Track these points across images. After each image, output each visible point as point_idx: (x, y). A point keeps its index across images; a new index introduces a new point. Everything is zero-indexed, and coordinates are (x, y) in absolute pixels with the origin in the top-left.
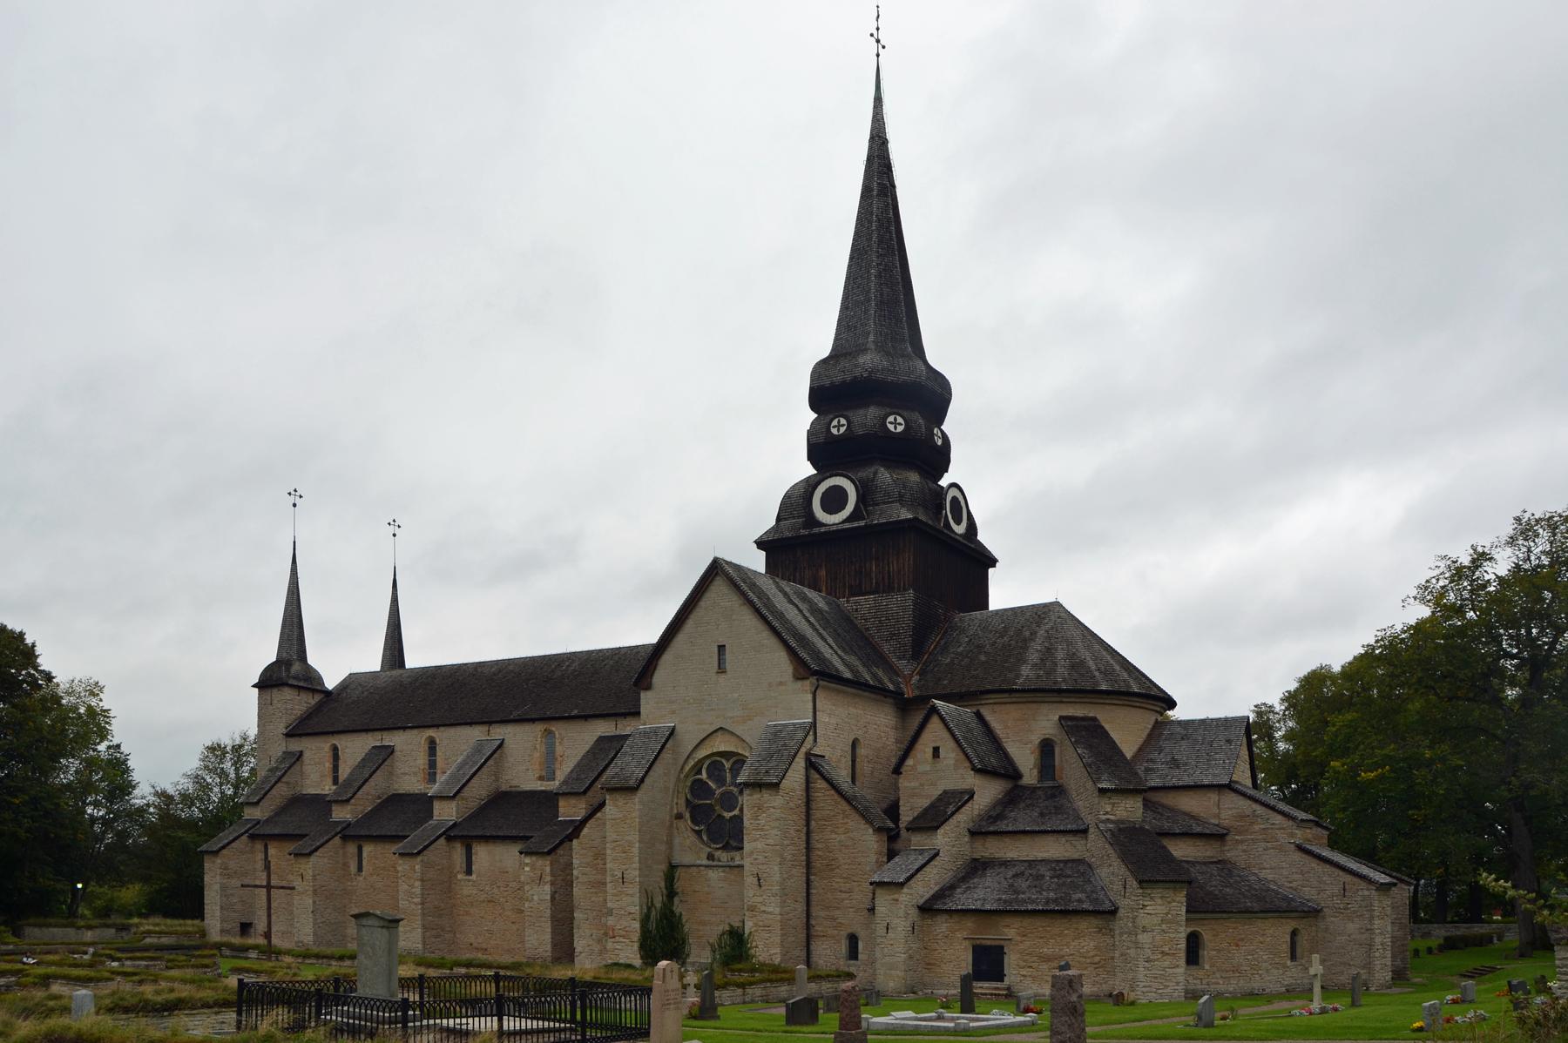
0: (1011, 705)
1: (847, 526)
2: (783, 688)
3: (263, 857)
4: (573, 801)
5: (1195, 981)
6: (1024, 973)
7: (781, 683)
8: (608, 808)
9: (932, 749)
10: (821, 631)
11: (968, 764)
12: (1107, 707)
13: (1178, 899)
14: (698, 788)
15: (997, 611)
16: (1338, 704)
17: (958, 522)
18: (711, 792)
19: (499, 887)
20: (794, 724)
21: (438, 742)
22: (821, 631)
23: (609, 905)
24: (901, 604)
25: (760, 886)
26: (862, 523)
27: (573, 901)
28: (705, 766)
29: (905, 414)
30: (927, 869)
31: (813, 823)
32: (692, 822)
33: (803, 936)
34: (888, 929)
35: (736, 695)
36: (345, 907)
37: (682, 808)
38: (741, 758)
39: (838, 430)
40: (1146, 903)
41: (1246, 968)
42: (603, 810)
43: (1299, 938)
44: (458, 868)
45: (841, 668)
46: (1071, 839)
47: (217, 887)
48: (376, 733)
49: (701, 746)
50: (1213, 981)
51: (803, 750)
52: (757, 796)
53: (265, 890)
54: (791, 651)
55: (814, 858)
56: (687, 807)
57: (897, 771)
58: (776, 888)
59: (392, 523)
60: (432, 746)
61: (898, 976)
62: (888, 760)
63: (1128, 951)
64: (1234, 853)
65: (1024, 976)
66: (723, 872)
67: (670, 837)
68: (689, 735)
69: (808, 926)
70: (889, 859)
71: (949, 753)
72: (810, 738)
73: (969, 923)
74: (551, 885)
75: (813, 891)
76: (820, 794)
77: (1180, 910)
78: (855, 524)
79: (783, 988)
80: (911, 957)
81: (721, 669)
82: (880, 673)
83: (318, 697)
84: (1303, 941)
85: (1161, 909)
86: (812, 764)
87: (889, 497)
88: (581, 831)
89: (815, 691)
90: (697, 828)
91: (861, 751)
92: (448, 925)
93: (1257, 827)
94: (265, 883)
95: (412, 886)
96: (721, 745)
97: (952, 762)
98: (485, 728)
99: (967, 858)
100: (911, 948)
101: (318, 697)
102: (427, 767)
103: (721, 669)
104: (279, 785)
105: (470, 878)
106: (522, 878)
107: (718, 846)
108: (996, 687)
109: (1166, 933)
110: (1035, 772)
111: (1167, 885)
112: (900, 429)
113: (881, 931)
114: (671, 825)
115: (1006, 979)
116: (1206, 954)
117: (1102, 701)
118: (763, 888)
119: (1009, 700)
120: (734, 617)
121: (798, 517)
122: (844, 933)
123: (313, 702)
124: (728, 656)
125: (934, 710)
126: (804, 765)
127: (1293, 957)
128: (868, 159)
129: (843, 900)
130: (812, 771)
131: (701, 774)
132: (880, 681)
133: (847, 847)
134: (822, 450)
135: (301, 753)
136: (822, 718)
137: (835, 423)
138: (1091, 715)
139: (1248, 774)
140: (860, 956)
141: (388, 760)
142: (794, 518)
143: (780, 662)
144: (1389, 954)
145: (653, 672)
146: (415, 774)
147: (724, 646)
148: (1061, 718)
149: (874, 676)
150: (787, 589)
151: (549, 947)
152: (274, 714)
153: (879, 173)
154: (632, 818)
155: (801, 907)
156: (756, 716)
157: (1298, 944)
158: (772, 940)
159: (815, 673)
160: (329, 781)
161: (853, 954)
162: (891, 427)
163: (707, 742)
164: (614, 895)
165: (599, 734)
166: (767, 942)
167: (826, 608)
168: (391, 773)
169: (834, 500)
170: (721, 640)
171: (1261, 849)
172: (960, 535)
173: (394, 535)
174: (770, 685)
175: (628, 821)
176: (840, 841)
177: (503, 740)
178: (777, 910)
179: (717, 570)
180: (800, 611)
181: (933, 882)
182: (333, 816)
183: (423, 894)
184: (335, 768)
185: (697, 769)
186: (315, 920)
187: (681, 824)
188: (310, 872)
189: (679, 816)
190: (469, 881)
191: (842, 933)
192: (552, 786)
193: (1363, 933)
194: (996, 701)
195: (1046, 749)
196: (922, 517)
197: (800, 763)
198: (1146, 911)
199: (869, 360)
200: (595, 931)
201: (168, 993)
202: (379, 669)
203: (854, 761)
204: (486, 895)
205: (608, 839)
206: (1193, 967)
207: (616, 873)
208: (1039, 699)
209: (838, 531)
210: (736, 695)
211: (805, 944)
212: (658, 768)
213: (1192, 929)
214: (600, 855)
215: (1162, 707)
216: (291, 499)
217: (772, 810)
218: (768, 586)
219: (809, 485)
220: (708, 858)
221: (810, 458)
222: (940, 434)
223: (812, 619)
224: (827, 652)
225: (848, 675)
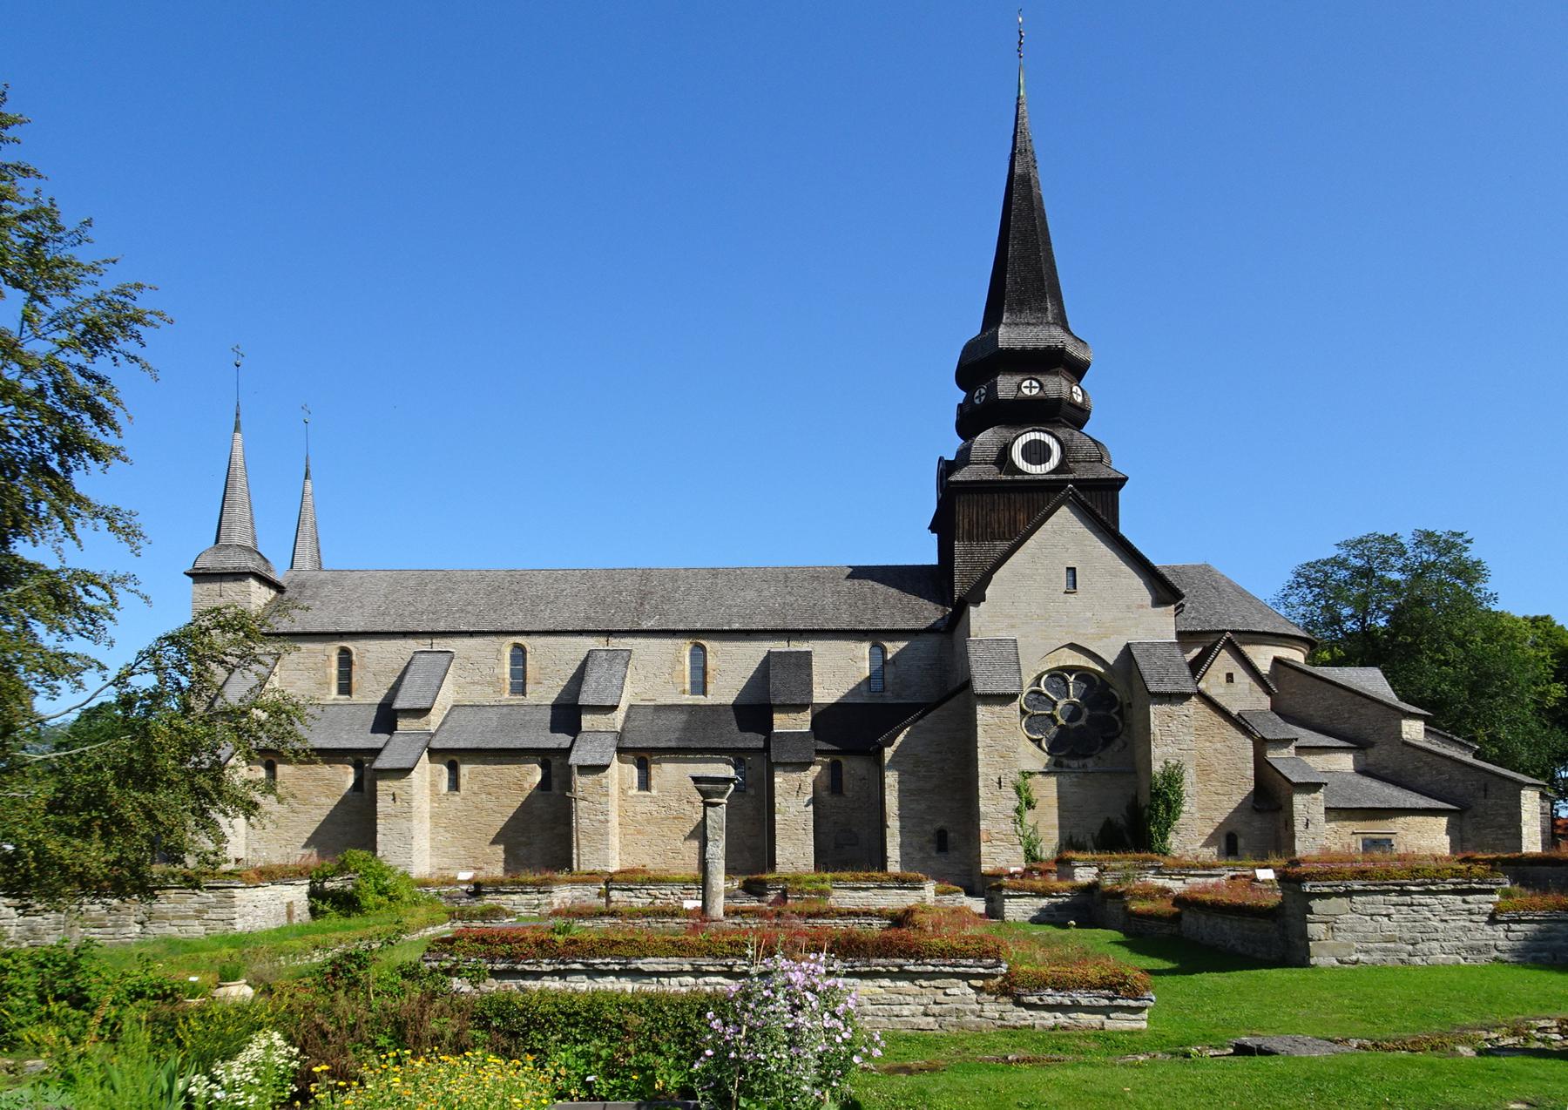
1: (1054, 477)
7: (1142, 606)
29: (1039, 378)
39: (1031, 391)
66: (1077, 777)
113: (1299, 826)
131: (1070, 676)
174: (1128, 607)
182: (399, 727)
209: (1044, 481)
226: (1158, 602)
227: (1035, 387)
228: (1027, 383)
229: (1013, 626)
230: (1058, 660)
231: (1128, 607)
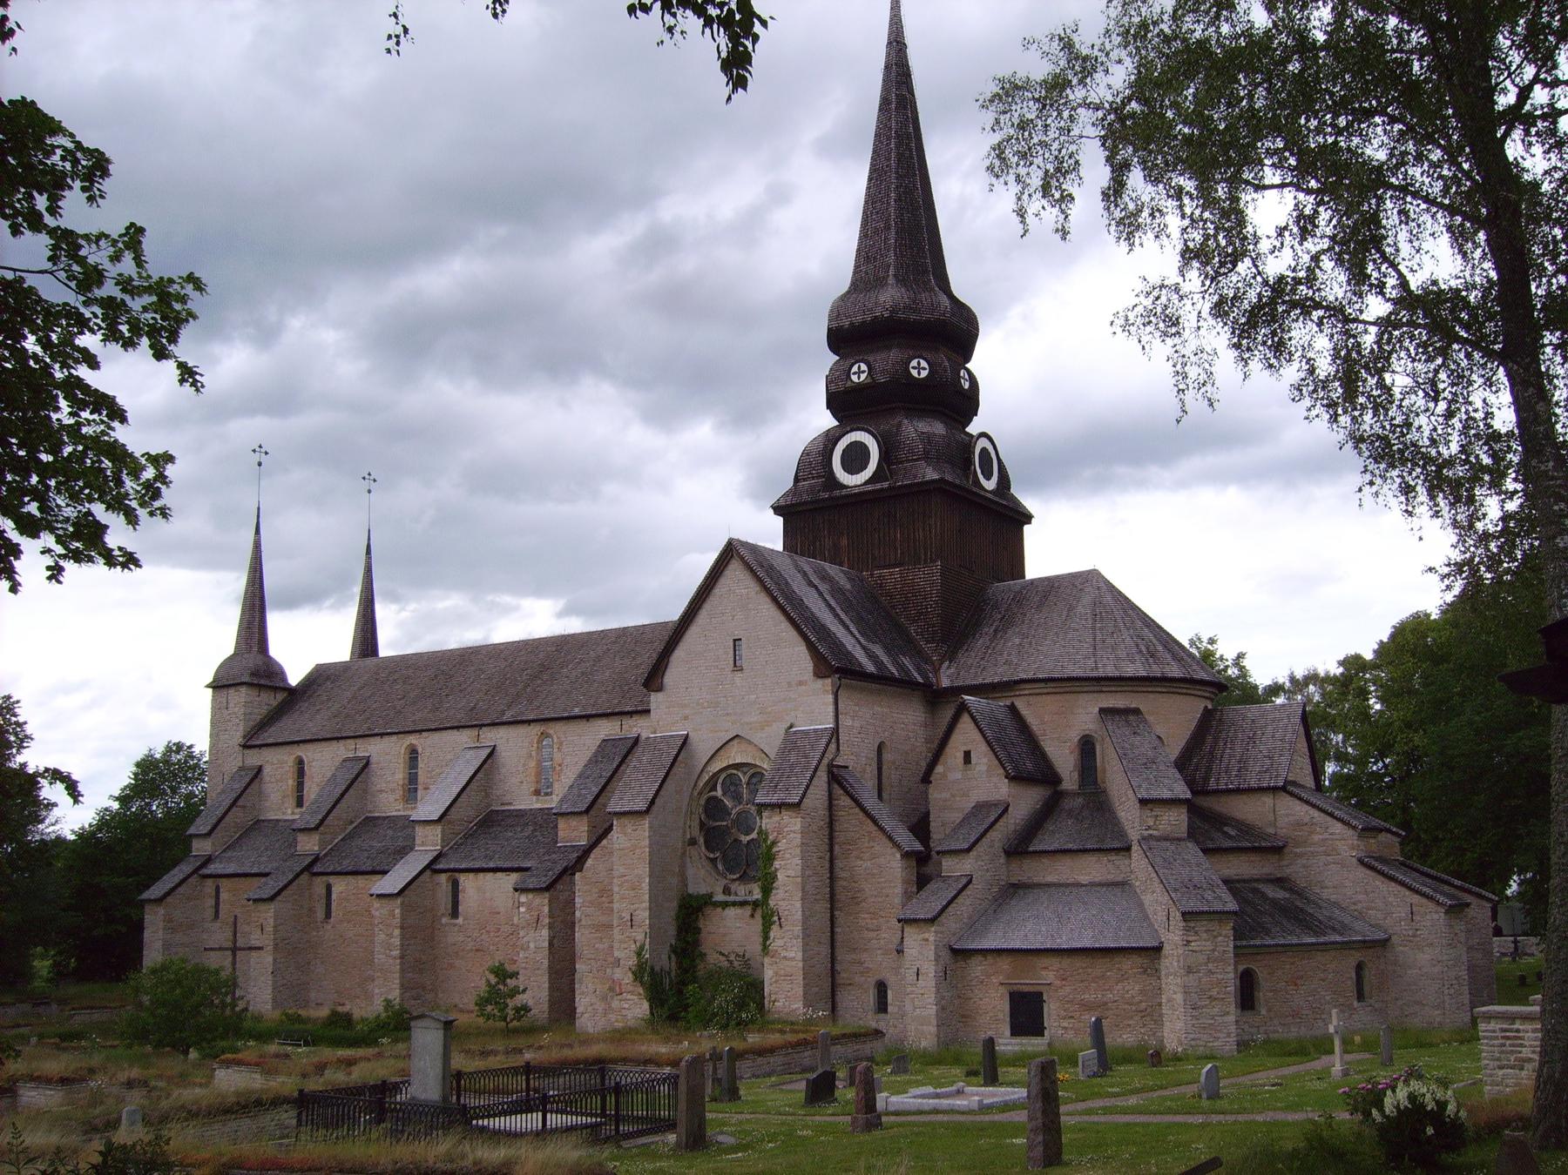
0: (1049, 697)
1: (870, 488)
3: (214, 903)
4: (574, 822)
5: (1250, 1030)
6: (1065, 1024)
7: (801, 683)
8: (614, 834)
10: (843, 616)
11: (1002, 771)
12: (1152, 696)
13: (1224, 933)
14: (713, 808)
16: (1435, 657)
17: (988, 478)
18: (725, 812)
19: (488, 932)
20: (816, 731)
21: (420, 750)
22: (843, 616)
23: (616, 954)
24: (928, 577)
26: (886, 485)
27: (574, 947)
28: (720, 781)
30: (960, 899)
31: (837, 848)
32: (707, 848)
33: (827, 985)
34: (918, 974)
35: (753, 697)
36: (309, 963)
37: (696, 832)
38: (759, 770)
40: (1190, 938)
41: (1307, 1012)
42: (609, 837)
43: (1366, 973)
44: (442, 910)
45: (894, 671)
46: (1114, 858)
47: (159, 944)
48: (349, 741)
50: (1271, 1028)
51: (825, 761)
52: (776, 818)
53: (230, 953)
54: (811, 646)
55: (838, 890)
56: (701, 830)
57: (926, 779)
58: (798, 929)
59: (367, 477)
60: (413, 755)
61: (930, 1034)
62: (917, 764)
63: (1174, 996)
64: (1293, 869)
65: (1065, 1028)
67: (683, 867)
68: (703, 746)
69: (833, 972)
70: (919, 889)
71: (983, 758)
72: (833, 746)
73: (1005, 964)
74: (550, 928)
75: (837, 930)
76: (843, 813)
77: (1228, 946)
78: (878, 486)
79: (806, 1054)
80: (943, 1009)
81: (737, 667)
82: (906, 661)
83: (280, 696)
84: (1370, 976)
85: (1209, 945)
86: (837, 777)
89: (837, 691)
90: (712, 856)
91: (887, 756)
92: (429, 983)
93: (1316, 838)
94: (229, 945)
95: (391, 936)
96: (736, 755)
98: (474, 732)
99: (1004, 883)
100: (943, 998)
101: (280, 696)
102: (406, 782)
103: (737, 667)
104: (234, 809)
105: (457, 921)
106: (516, 920)
107: (735, 877)
108: (1030, 676)
109: (1213, 973)
110: (1076, 775)
111: (1212, 917)
112: (924, 374)
114: (684, 854)
115: (1046, 1033)
116: (1262, 995)
117: (1145, 689)
118: (784, 929)
119: (1045, 691)
121: (818, 477)
122: (872, 981)
123: (275, 703)
124: (744, 650)
125: (963, 708)
126: (826, 780)
127: (1360, 996)
128: (886, 67)
130: (836, 786)
131: (716, 790)
132: (907, 672)
134: (842, 401)
135: (260, 769)
136: (846, 721)
137: (855, 369)
138: (1133, 706)
139: (1308, 769)
140: (890, 1009)
141: (362, 776)
142: (813, 478)
143: (797, 657)
144: (1466, 989)
145: (663, 674)
146: (393, 790)
148: (1102, 711)
149: (901, 667)
150: (807, 568)
151: (546, 1007)
152: (230, 721)
153: (897, 82)
155: (825, 950)
157: (1366, 981)
158: (794, 991)
159: (837, 670)
160: (291, 802)
161: (882, 1006)
162: (914, 373)
165: (602, 737)
167: (848, 586)
168: (365, 791)
169: (857, 455)
171: (1321, 864)
172: (990, 492)
173: (369, 491)
177: (495, 746)
178: (800, 955)
179: (732, 552)
180: (820, 594)
181: (965, 915)
183: (402, 945)
184: (300, 786)
185: (712, 784)
186: (275, 982)
187: (693, 851)
188: (271, 921)
189: (693, 842)
190: (455, 925)
192: (552, 802)
193: (1434, 966)
194: (1031, 691)
195: (1087, 747)
196: (948, 477)
197: (822, 776)
198: (1191, 948)
199: (890, 296)
202: (348, 659)
203: (880, 769)
204: (472, 943)
205: (616, 873)
206: (1249, 1012)
207: (623, 915)
210: (753, 697)
211: (829, 994)
212: (670, 785)
213: (1245, 967)
214: (605, 892)
215: (1212, 693)
216: (256, 457)
218: (786, 567)
219: (830, 439)
220: (724, 892)
221: (829, 406)
222: (967, 377)
223: (833, 603)
224: (849, 642)
225: (870, 668)
227: (924, 369)
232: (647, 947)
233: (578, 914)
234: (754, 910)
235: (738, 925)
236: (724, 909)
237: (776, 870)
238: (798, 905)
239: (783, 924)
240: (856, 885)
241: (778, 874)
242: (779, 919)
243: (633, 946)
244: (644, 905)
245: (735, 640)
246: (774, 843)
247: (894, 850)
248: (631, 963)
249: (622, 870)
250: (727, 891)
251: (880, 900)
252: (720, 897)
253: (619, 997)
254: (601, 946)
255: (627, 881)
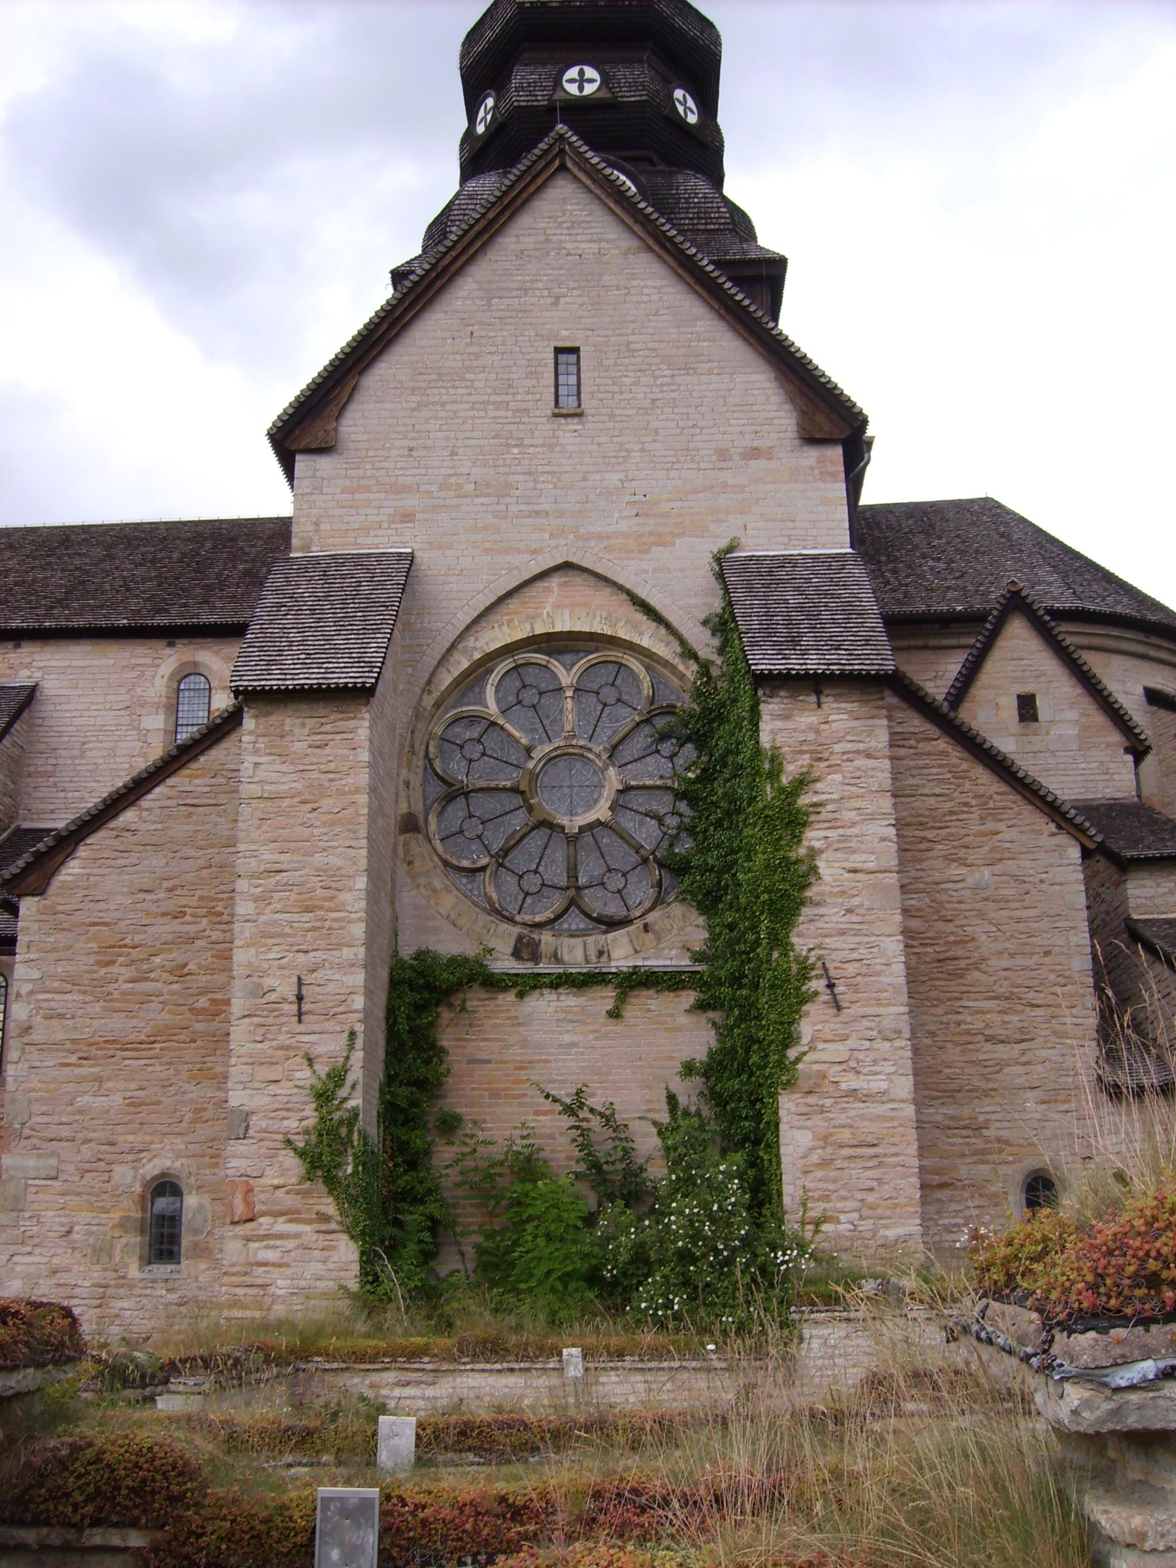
2: (762, 463)
7: (755, 453)
9: (1015, 703)
15: (871, 506)
23: (237, 1098)
25: (839, 1008)
35: (614, 478)
39: (581, 88)
49: (492, 617)
58: (895, 1012)
87: (709, 220)
88: (56, 870)
97: (1073, 731)
120: (606, 279)
129: (1001, 1065)
133: (1002, 902)
145: (343, 408)
147: (575, 351)
154: (341, 793)
156: (682, 535)
163: (513, 604)
164: (256, 1062)
166: (870, 1198)
170: (564, 333)
174: (723, 455)
175: (326, 803)
176: (976, 888)
191: (1003, 1170)
200: (84, 1216)
201: (940, 1390)
207: (269, 982)
208: (1111, 643)
210: (614, 478)
217: (861, 762)
226: (811, 439)
228: (573, 73)
229: (407, 517)
230: (532, 618)
231: (723, 455)
232: (356, 1074)
233: (19, 1011)
234: (622, 999)
235: (567, 1038)
236: (521, 995)
237: (813, 853)
238: (894, 946)
239: (844, 1000)
240: (950, 927)
241: (821, 864)
242: (831, 986)
243: (307, 1073)
244: (347, 953)
245: (558, 351)
246: (802, 783)
247: (1063, 839)
248: (292, 1124)
249: (268, 855)
250: (525, 949)
251: (1030, 962)
252: (504, 964)
253: (241, 1230)
254: (99, 1103)
255: (289, 886)
